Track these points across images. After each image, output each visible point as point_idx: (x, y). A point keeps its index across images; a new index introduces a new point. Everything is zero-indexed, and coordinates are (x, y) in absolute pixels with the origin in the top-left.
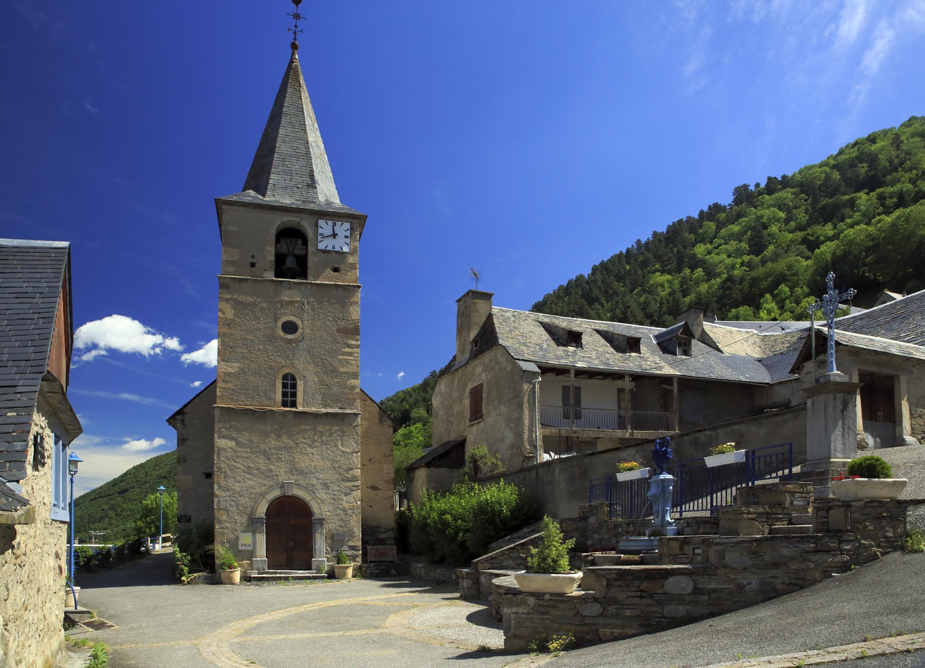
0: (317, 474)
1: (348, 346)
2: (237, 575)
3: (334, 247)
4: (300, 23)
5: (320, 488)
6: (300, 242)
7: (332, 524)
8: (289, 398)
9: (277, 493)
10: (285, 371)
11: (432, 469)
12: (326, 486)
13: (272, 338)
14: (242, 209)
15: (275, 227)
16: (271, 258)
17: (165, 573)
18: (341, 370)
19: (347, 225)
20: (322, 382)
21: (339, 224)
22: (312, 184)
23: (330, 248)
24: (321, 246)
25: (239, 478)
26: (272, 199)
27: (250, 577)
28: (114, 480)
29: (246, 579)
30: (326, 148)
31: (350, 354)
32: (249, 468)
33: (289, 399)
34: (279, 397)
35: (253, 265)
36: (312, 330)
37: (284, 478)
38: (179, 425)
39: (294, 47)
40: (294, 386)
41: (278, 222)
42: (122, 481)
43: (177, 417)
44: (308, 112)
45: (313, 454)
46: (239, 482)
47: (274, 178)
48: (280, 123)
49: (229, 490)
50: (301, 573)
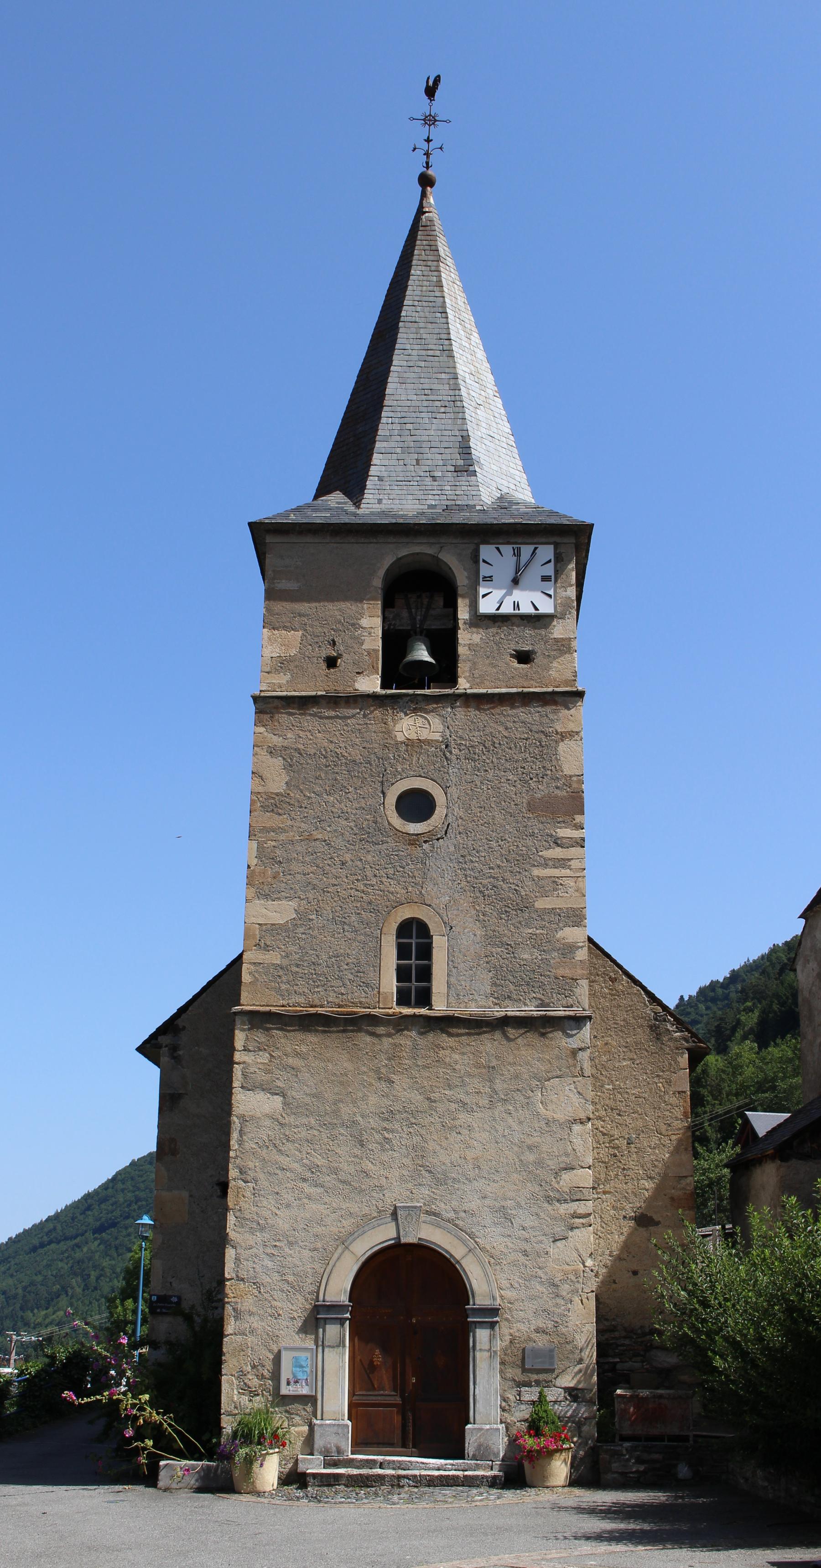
0: (479, 1184)
2: (269, 1472)
3: (516, 606)
5: (488, 1221)
6: (440, 601)
7: (523, 1322)
8: (415, 981)
9: (381, 1235)
10: (405, 913)
11: (794, 1162)
12: (504, 1215)
13: (372, 832)
14: (309, 539)
15: (381, 573)
16: (374, 642)
17: (123, 1464)
18: (540, 904)
19: (546, 552)
20: (492, 939)
22: (466, 466)
24: (487, 606)
26: (377, 508)
27: (304, 1475)
28: (88, 1197)
29: (294, 1478)
30: (497, 383)
31: (562, 863)
32: (313, 1168)
33: (414, 984)
34: (390, 984)
35: (331, 662)
37: (396, 1194)
38: (165, 1059)
39: (426, 181)
40: (426, 952)
41: (388, 561)
42: (104, 1200)
43: (162, 1039)
44: (456, 310)
46: (288, 1206)
47: (379, 464)
48: (394, 342)
49: (262, 1229)
50: (434, 1466)
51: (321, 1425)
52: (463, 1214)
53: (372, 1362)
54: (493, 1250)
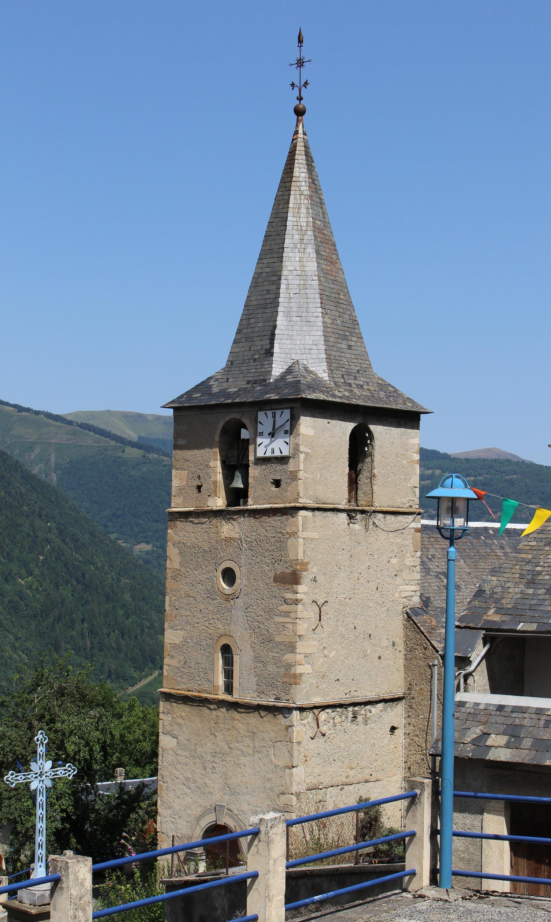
13: (212, 593)
19: (287, 414)
20: (257, 659)
21: (278, 413)
23: (269, 454)
34: (221, 680)
35: (199, 488)
49: (169, 808)
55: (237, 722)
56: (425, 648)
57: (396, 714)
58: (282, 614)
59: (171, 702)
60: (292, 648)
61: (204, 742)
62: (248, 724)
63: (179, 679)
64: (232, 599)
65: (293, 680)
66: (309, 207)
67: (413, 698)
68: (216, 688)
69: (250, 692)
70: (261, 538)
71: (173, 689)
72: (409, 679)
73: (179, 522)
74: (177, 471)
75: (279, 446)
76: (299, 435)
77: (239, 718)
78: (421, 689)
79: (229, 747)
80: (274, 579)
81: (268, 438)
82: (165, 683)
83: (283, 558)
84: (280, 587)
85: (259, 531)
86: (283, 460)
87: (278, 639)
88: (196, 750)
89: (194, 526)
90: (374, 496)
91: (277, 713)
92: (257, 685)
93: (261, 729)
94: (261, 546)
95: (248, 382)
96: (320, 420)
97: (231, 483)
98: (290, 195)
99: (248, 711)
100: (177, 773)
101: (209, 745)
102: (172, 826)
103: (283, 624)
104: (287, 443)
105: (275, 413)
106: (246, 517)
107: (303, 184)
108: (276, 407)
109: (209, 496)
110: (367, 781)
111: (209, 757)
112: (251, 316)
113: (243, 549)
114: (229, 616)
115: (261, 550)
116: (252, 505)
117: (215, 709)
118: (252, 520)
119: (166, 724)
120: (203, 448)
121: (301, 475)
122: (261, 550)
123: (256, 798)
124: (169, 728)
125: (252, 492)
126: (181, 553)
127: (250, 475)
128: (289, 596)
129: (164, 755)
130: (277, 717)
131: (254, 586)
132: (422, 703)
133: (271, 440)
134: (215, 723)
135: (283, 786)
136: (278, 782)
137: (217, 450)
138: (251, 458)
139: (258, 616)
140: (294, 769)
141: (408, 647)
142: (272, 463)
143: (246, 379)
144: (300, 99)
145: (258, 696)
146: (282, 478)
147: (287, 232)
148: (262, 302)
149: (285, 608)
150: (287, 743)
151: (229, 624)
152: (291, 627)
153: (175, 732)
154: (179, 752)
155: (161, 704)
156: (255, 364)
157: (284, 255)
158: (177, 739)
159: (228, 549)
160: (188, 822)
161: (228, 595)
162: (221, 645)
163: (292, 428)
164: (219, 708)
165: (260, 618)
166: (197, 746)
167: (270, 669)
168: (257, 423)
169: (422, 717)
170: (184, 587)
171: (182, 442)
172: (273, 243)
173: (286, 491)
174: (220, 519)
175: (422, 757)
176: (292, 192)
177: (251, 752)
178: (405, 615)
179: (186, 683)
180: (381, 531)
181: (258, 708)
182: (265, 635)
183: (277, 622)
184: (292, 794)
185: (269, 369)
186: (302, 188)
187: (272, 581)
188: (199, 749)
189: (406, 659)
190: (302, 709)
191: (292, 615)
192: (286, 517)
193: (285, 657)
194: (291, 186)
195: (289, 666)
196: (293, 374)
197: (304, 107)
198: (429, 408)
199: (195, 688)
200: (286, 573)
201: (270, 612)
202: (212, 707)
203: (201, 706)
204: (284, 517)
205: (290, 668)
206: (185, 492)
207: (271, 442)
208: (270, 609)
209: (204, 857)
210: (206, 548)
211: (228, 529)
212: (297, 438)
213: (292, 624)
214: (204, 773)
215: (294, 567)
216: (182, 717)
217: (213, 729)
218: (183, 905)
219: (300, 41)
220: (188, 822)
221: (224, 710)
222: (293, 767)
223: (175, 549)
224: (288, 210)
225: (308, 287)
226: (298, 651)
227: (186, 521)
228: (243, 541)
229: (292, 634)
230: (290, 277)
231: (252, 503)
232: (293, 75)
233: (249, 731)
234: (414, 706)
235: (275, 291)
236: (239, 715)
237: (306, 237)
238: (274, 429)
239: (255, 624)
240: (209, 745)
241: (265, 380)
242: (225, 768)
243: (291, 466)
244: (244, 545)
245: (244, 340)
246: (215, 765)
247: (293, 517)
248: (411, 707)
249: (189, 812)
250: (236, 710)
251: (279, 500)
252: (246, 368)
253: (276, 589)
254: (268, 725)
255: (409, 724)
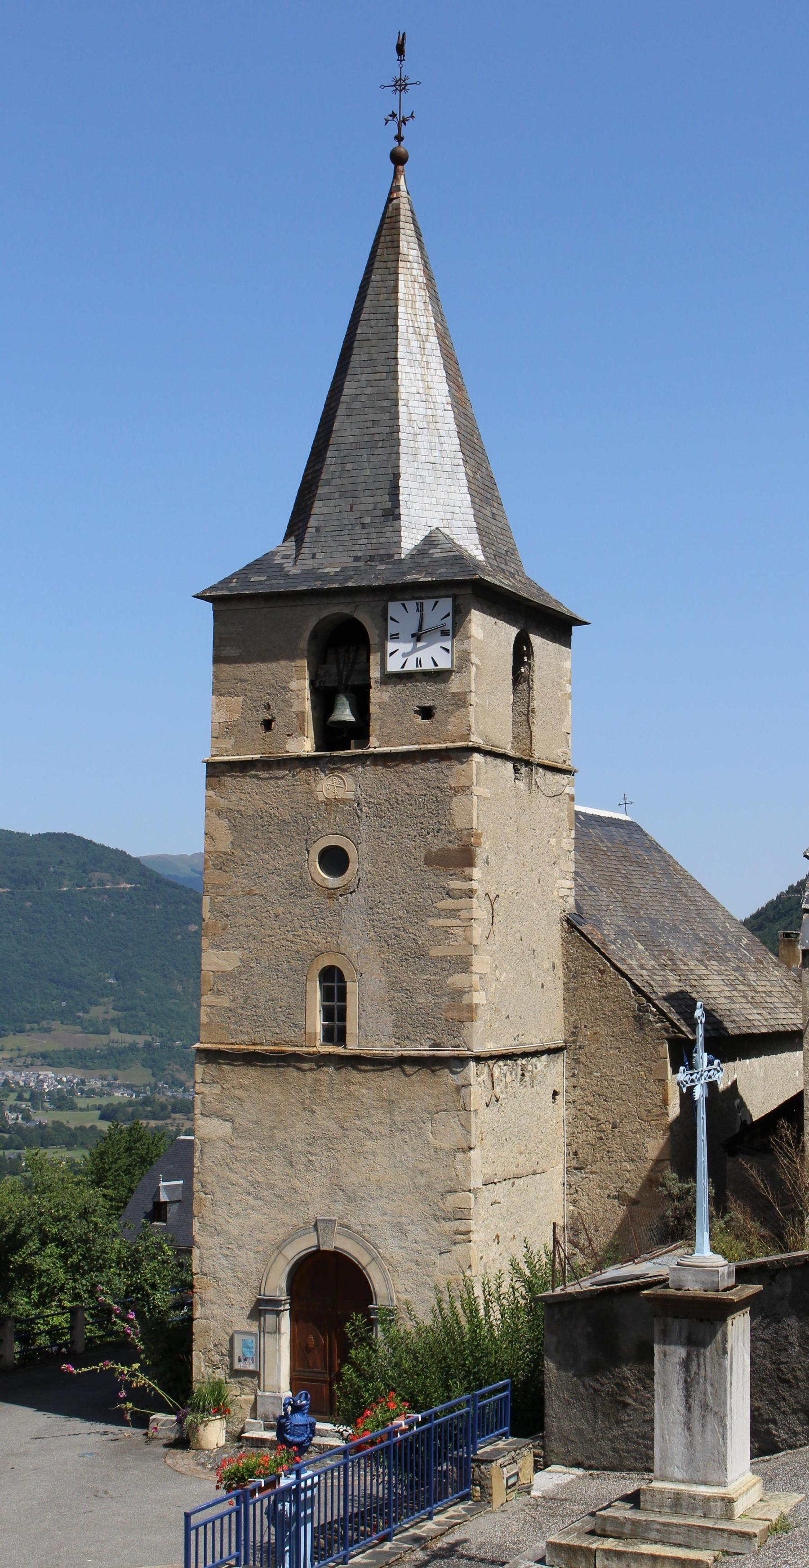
0: (381, 1203)
1: (449, 894)
4: (410, 102)
9: (306, 1244)
12: (400, 1230)
13: (299, 888)
19: (446, 605)
20: (394, 985)
21: (428, 604)
23: (411, 667)
25: (237, 1208)
34: (317, 1024)
35: (268, 725)
36: (375, 863)
41: (313, 623)
45: (374, 1153)
49: (219, 1234)
51: (262, 1396)
52: (368, 1228)
53: (307, 1345)
54: (391, 1260)
55: (357, 1087)
56: (602, 972)
57: (553, 1073)
58: (443, 913)
59: (219, 1064)
60: (464, 965)
61: (290, 1122)
62: (379, 1088)
63: (232, 1027)
64: (341, 895)
65: (466, 1015)
66: (428, 301)
67: (580, 1048)
68: (309, 1038)
69: (381, 1037)
70: (399, 797)
71: (221, 1043)
72: (572, 1019)
73: (229, 779)
74: (222, 698)
75: (434, 655)
76: (468, 638)
77: (361, 1080)
78: (595, 1033)
79: (342, 1127)
80: (426, 858)
81: (409, 642)
82: (203, 1035)
83: (443, 827)
84: (438, 872)
85: (393, 787)
86: (438, 676)
87: (436, 952)
88: (272, 1137)
89: (260, 783)
90: (534, 741)
91: (437, 1068)
92: (396, 1026)
93: (407, 1094)
94: (400, 810)
95: (357, 559)
96: (488, 618)
97: (330, 715)
98: (397, 280)
99: (380, 1068)
100: (233, 1177)
101: (300, 1127)
102: (225, 1263)
103: (445, 929)
104: (447, 650)
105: (422, 604)
106: (367, 766)
107: (415, 265)
108: (423, 595)
109: (288, 735)
110: (534, 1173)
111: (300, 1146)
112: (346, 460)
113: (364, 816)
114: (335, 921)
115: (398, 816)
116: (375, 745)
117: (311, 1070)
118: (380, 770)
119: (209, 1099)
120: (275, 658)
121: (473, 698)
122: (398, 816)
123: (399, 1202)
124: (215, 1105)
125: (377, 727)
126: (235, 827)
127: (372, 700)
128: (456, 884)
129: (205, 1150)
130: (439, 1073)
131: (387, 872)
132: (598, 1053)
133: (415, 646)
134: (311, 1092)
135: (451, 1179)
136: (441, 1174)
137: (305, 663)
138: (375, 674)
139: (394, 919)
140: (472, 1152)
141: (570, 972)
142: (417, 681)
143: (352, 554)
144: (399, 138)
145: (397, 1044)
146: (436, 704)
147: (400, 335)
148: (366, 438)
149: (449, 903)
150: (459, 1113)
151: (336, 935)
152: (461, 933)
153: (229, 1111)
154: (238, 1142)
155: (199, 1069)
156: (364, 531)
157: (399, 368)
158: (233, 1122)
159: (332, 817)
160: (258, 1252)
161: (334, 889)
162: (321, 968)
163: (456, 626)
164: (319, 1067)
165: (399, 921)
166: (275, 1131)
167: (421, 1001)
168: (386, 620)
169: (598, 1074)
170: (240, 881)
171: (228, 651)
172: (373, 350)
173: (445, 723)
174: (315, 770)
175: (598, 1134)
176: (401, 277)
177: (385, 1131)
178: (564, 923)
179: (247, 1033)
180: (541, 794)
181: (401, 1061)
182: (409, 947)
183: (433, 926)
184: (470, 1191)
185: (396, 539)
186: (415, 272)
187: (422, 864)
188: (279, 1135)
189: (566, 989)
190: (478, 1059)
191: (463, 914)
192: (448, 763)
193: (450, 980)
194: (397, 267)
195: (460, 993)
196: (439, 546)
197: (406, 152)
198: (581, 616)
199: (268, 1038)
200: (449, 850)
201: (420, 912)
202: (305, 1066)
203: (283, 1067)
204: (444, 764)
205: (460, 996)
206: (239, 731)
207: (415, 650)
208: (419, 907)
209: (288, 1306)
210: (287, 818)
211: (328, 786)
212: (466, 642)
213: (462, 929)
214: (289, 1172)
215: (465, 839)
216: (242, 1087)
217: (307, 1102)
218: (590, 1329)
219: (400, 49)
220: (258, 1252)
221: (331, 1069)
222: (471, 1149)
223: (222, 821)
224: (397, 302)
225: (438, 419)
226: (474, 969)
227: (244, 776)
228: (363, 803)
229: (465, 943)
230: (411, 403)
231: (377, 744)
232: (390, 102)
233: (382, 1100)
234: (583, 1059)
235: (390, 423)
236: (363, 1075)
237: (427, 345)
238: (420, 629)
239: (389, 932)
240: (300, 1127)
241: (392, 556)
242: (333, 1162)
243: (455, 685)
244: (365, 809)
245: (337, 495)
246: (313, 1158)
247: (463, 763)
248: (577, 1061)
249: (260, 1236)
250: (354, 1068)
251: (432, 738)
252: (348, 537)
253: (430, 875)
254: (420, 1089)
255: (575, 1087)
